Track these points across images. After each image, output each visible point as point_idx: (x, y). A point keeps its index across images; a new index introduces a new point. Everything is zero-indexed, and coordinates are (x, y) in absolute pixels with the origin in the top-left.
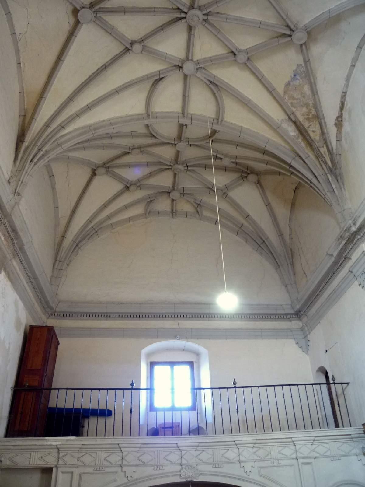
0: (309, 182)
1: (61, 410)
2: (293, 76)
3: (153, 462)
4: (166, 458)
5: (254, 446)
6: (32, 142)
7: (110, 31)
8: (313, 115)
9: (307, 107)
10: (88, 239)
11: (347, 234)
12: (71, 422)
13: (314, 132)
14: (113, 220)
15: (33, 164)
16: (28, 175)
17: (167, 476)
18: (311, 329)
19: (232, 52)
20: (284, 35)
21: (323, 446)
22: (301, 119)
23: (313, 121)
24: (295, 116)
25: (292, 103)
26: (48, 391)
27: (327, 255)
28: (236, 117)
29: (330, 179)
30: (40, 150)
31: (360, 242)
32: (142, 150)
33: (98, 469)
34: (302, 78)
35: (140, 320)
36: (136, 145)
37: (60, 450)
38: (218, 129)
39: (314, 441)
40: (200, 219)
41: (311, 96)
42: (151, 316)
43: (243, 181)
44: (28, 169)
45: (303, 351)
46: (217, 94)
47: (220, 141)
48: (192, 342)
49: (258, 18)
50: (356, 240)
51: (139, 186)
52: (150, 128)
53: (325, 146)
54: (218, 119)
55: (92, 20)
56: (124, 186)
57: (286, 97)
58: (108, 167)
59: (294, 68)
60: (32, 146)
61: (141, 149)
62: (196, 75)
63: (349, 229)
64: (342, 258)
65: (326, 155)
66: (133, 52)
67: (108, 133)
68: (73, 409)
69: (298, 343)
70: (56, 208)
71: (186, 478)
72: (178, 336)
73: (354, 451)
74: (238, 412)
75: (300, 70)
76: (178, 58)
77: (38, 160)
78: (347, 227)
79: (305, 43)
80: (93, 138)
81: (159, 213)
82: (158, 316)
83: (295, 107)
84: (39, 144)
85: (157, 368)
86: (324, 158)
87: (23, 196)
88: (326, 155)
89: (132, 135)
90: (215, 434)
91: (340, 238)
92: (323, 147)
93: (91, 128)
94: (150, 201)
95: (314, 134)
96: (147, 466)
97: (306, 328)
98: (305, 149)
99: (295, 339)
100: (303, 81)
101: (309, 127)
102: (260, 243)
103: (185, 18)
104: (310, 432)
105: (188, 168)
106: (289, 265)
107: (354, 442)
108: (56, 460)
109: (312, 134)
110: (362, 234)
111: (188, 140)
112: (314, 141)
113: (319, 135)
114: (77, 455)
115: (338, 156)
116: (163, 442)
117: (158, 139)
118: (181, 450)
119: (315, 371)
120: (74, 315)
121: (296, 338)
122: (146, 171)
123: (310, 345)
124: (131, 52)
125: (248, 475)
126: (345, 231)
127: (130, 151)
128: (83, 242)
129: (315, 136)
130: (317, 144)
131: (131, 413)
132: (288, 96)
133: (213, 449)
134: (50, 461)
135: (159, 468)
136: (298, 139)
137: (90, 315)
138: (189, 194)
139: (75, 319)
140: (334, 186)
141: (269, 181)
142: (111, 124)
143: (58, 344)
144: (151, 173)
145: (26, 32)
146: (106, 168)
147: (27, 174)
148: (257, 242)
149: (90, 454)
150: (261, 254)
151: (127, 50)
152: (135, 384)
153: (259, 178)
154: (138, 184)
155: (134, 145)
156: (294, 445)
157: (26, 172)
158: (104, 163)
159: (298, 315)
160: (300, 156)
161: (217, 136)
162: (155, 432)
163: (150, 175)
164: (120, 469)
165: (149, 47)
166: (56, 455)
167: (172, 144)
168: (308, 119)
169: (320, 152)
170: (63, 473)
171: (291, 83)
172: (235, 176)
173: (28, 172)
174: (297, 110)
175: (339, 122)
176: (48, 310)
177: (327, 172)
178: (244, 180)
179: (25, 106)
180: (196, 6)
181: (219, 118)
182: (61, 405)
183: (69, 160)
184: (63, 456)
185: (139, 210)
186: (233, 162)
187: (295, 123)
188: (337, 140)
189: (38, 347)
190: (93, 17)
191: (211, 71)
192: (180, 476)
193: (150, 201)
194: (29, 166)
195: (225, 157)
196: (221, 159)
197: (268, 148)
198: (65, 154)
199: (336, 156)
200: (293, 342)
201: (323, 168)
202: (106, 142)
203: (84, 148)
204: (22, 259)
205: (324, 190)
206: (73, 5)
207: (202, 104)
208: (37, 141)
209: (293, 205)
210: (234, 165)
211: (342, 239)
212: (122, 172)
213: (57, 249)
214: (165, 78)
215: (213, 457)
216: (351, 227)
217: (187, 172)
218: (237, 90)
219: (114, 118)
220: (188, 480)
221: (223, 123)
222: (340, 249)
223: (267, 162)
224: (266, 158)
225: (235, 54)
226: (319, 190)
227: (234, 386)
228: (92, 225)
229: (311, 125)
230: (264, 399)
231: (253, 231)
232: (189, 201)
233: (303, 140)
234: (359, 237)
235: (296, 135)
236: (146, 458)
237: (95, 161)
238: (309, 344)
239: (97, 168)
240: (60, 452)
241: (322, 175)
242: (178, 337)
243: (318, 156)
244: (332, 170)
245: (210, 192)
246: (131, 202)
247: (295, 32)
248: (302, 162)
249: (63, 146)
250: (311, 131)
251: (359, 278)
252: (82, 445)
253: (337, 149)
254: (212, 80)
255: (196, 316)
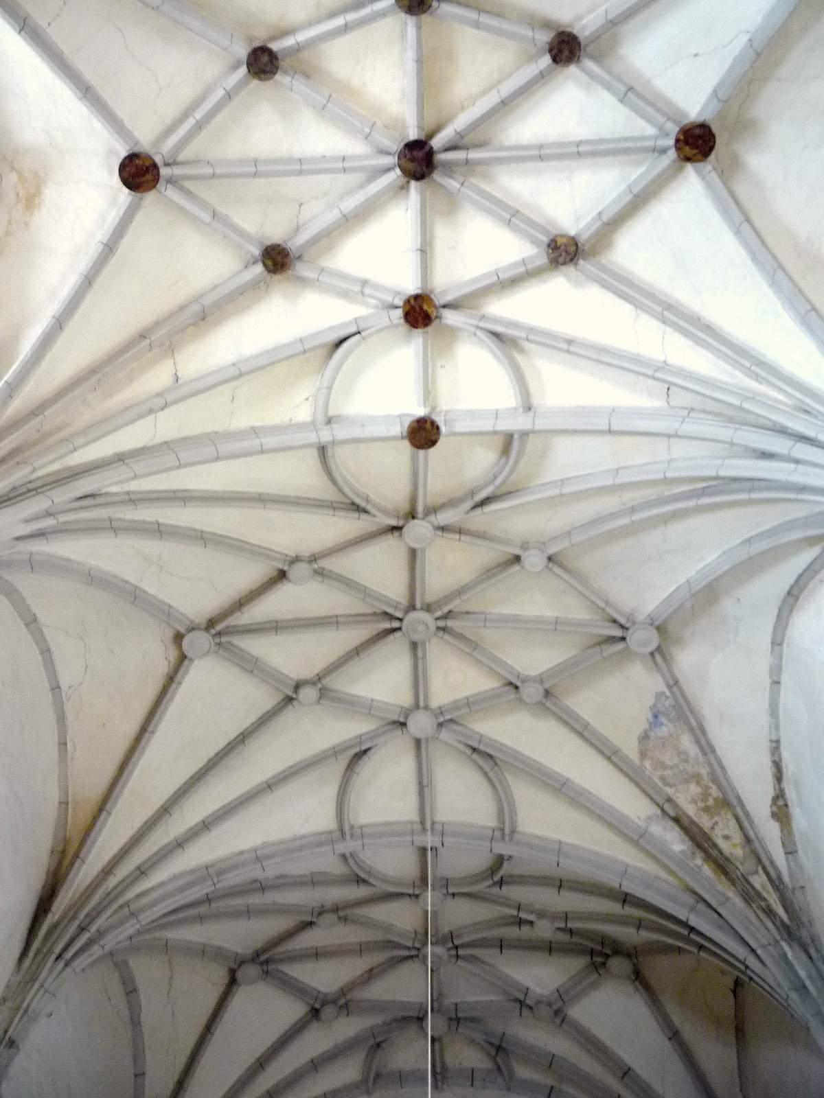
2: (651, 719)
6: (69, 910)
7: (252, 666)
8: (715, 799)
9: (698, 783)
13: (727, 838)
15: (61, 964)
19: (511, 684)
20: (612, 640)
22: (690, 810)
23: (719, 814)
24: (676, 806)
25: (663, 778)
28: (544, 821)
29: (790, 954)
30: (82, 929)
32: (342, 914)
34: (671, 721)
36: (328, 905)
40: (509, 1089)
41: (701, 759)
44: (46, 979)
46: (491, 774)
47: (522, 880)
49: (549, 613)
51: (346, 1005)
52: (351, 861)
53: (760, 869)
54: (502, 830)
55: (210, 649)
56: (309, 1008)
57: (647, 764)
58: (267, 962)
59: (650, 701)
61: (341, 912)
62: (439, 738)
66: (300, 703)
67: (255, 881)
75: (664, 706)
76: (397, 706)
79: (659, 649)
80: (214, 897)
83: (671, 786)
84: (82, 916)
86: (765, 900)
88: (768, 892)
89: (313, 881)
92: (756, 872)
93: (211, 871)
100: (675, 726)
101: (713, 828)
103: (399, 629)
109: (724, 845)
111: (446, 882)
112: (732, 859)
113: (741, 844)
124: (295, 703)
129: (732, 847)
132: (650, 762)
138: (473, 1020)
142: (258, 859)
144: (371, 970)
145: (81, 683)
146: (262, 964)
151: (289, 700)
154: (343, 1002)
157: (42, 986)
160: (705, 901)
161: (506, 869)
163: (371, 975)
165: (336, 691)
167: (410, 895)
168: (706, 809)
169: (753, 887)
171: (652, 734)
172: (577, 964)
174: (677, 791)
175: (781, 811)
179: (68, 833)
180: (418, 605)
181: (505, 828)
183: (166, 948)
186: (559, 929)
187: (676, 820)
190: (213, 645)
191: (470, 726)
193: (376, 1044)
194: (51, 971)
196: (531, 923)
197: (628, 887)
198: (157, 934)
199: (793, 893)
201: (767, 929)
202: (255, 900)
203: (201, 919)
206: (173, 628)
207: (463, 799)
210: (564, 937)
214: (373, 751)
218: (535, 761)
219: (265, 845)
221: (517, 836)
224: (629, 911)
225: (517, 688)
229: (716, 823)
233: (705, 860)
235: (688, 849)
241: (770, 947)
243: (750, 896)
245: (521, 1010)
246: (328, 1051)
247: (631, 631)
248: (715, 915)
253: (791, 876)
254: (476, 745)
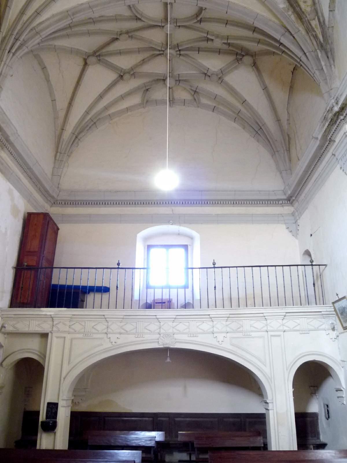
0: (299, 61)
1: (62, 287)
3: (134, 331)
4: (147, 328)
5: (174, 321)
6: (9, 31)
10: (88, 130)
11: (330, 115)
12: (71, 297)
14: (112, 110)
15: (11, 55)
16: (7, 66)
17: (146, 343)
18: (301, 214)
21: (293, 321)
26: (50, 270)
27: (312, 138)
29: (320, 55)
30: (16, 40)
31: (344, 123)
32: (130, 34)
33: (87, 335)
35: (135, 207)
37: (54, 319)
38: (204, 6)
39: (285, 316)
42: (146, 203)
43: (238, 64)
45: (293, 235)
48: (184, 227)
50: (339, 121)
51: (134, 74)
58: (99, 56)
60: (9, 36)
61: (129, 34)
63: (332, 109)
64: (327, 141)
65: (317, 28)
68: (66, 285)
69: (288, 228)
70: (54, 100)
71: (163, 344)
72: (171, 221)
73: (323, 327)
74: (215, 289)
77: (16, 51)
78: (330, 107)
81: (156, 102)
82: (164, 203)
85: (153, 250)
86: (315, 31)
87: (3, 88)
88: (317, 28)
89: (116, 19)
90: (131, 308)
91: (324, 120)
92: (314, 19)
93: (70, 13)
94: (146, 89)
95: (305, 4)
96: (129, 334)
97: (297, 214)
98: (295, 23)
99: (285, 223)
102: (258, 130)
104: (281, 309)
105: (180, 53)
106: (285, 151)
107: (324, 318)
108: (51, 327)
109: (303, 5)
110: (344, 115)
111: (176, 21)
112: (305, 13)
114: (68, 323)
115: (330, 29)
116: (144, 314)
117: (144, 21)
118: (160, 321)
119: (302, 253)
120: (74, 203)
121: (287, 223)
122: (140, 57)
123: (299, 230)
125: (220, 344)
126: (328, 112)
127: (118, 37)
128: (83, 134)
130: (308, 16)
131: (117, 289)
133: (85, 321)
134: (45, 328)
135: (140, 336)
136: (288, 12)
137: (97, 203)
138: (185, 81)
139: (76, 207)
140: (323, 63)
141: (265, 62)
143: (58, 229)
144: (143, 60)
146: (97, 56)
147: (6, 65)
148: (253, 128)
149: (80, 323)
150: (258, 141)
152: (121, 264)
153: (254, 60)
154: (132, 73)
155: (122, 30)
156: (265, 319)
157: (5, 64)
158: (94, 51)
159: (290, 200)
160: (290, 32)
161: (204, 15)
162: (149, 306)
163: (144, 62)
164: (105, 336)
166: (51, 323)
167: (160, 26)
169: (311, 25)
170: (57, 337)
173: (7, 64)
176: (49, 198)
177: (317, 48)
178: (239, 63)
182: (62, 282)
184: (56, 324)
185: (136, 99)
186: (224, 43)
188: (329, 11)
189: (38, 233)
192: (158, 343)
193: (146, 89)
195: (216, 38)
196: (212, 40)
197: (257, 24)
199: (328, 29)
200: (284, 226)
203: (68, 36)
204: (12, 153)
205: (312, 68)
208: (13, 31)
209: (291, 88)
210: (226, 47)
211: (325, 120)
212: (115, 61)
213: (57, 142)
215: (189, 328)
216: (333, 107)
217: (180, 56)
220: (165, 346)
222: (324, 131)
223: (258, 40)
224: (256, 36)
226: (308, 68)
227: (213, 266)
228: (89, 117)
230: (249, 279)
231: (250, 117)
232: (185, 89)
233: (293, 12)
234: (342, 117)
236: (128, 327)
237: (87, 51)
238: (298, 228)
239: (88, 57)
240: (54, 320)
241: (312, 52)
242: (171, 223)
243: (309, 30)
244: (323, 45)
245: (205, 77)
248: (292, 37)
249: (41, 34)
250: (302, 2)
251: (340, 161)
252: (73, 315)
253: (329, 21)
255: (206, 203)
